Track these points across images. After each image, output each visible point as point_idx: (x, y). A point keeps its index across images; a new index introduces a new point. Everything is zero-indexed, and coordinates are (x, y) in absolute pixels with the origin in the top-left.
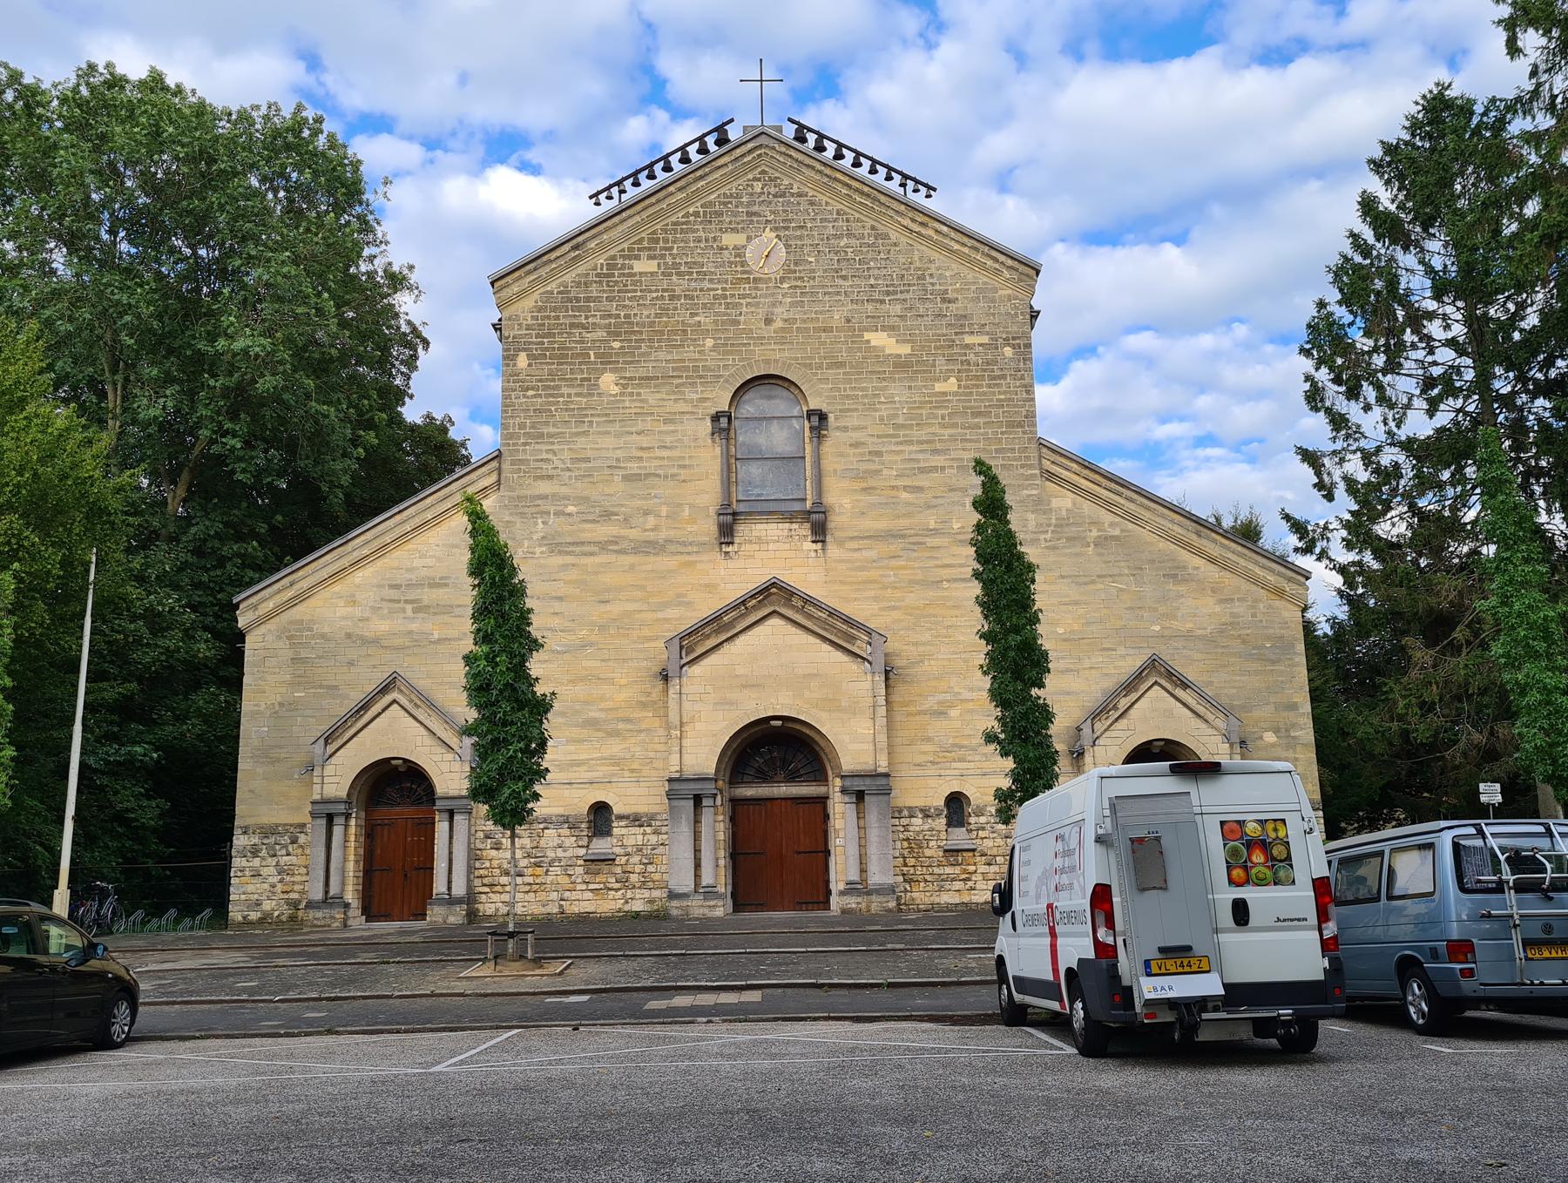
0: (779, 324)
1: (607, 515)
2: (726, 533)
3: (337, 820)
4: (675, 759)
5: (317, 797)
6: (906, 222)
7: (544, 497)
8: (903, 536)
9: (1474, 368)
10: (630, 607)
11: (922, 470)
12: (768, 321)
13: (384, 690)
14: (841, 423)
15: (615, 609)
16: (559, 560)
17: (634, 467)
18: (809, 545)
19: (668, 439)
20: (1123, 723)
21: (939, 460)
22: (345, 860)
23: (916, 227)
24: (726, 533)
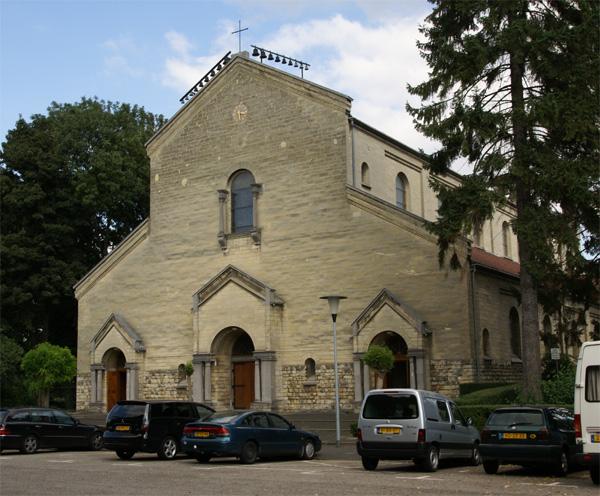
0: (244, 145)
1: (185, 241)
2: (222, 244)
3: (99, 372)
4: (195, 347)
5: (355, 351)
6: (292, 85)
7: (164, 236)
8: (290, 239)
9: (511, 101)
10: (192, 280)
11: (299, 206)
12: (240, 144)
13: (111, 321)
14: (268, 187)
15: (187, 281)
16: (169, 262)
17: (193, 219)
18: (254, 247)
19: (204, 205)
20: (371, 323)
21: (305, 200)
22: (103, 387)
23: (296, 87)
24: (222, 244)
